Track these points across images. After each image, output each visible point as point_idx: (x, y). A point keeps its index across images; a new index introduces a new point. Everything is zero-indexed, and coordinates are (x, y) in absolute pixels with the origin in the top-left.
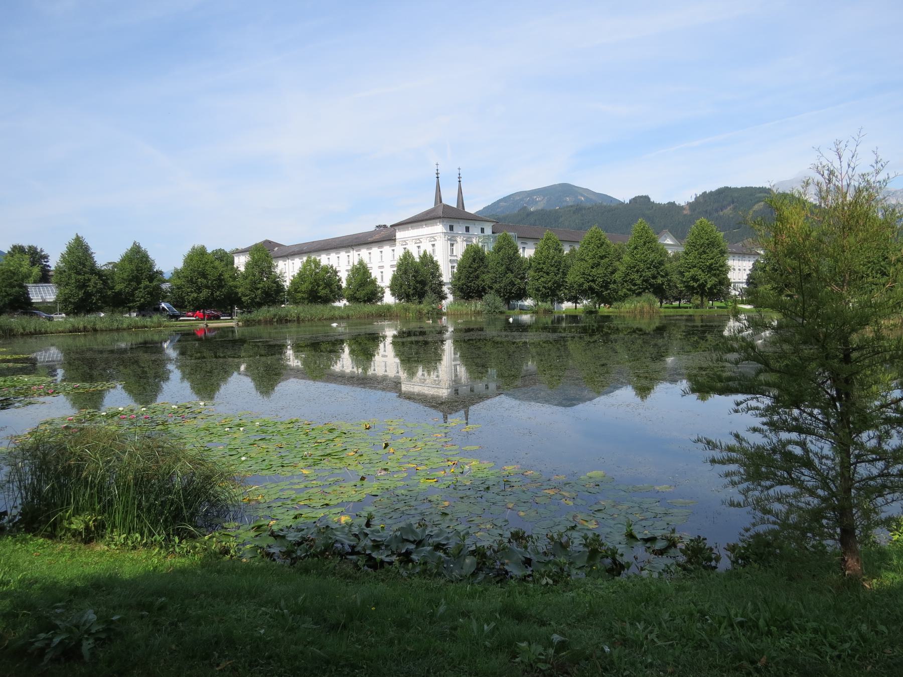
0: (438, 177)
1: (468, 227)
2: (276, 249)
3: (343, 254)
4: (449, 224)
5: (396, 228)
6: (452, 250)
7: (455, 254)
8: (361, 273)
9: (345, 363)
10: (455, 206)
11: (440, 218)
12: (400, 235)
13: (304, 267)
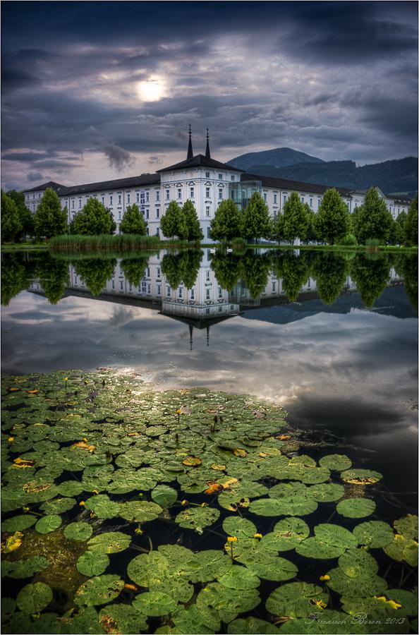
5: (161, 174)
6: (208, 195)
10: (194, 156)
12: (165, 179)
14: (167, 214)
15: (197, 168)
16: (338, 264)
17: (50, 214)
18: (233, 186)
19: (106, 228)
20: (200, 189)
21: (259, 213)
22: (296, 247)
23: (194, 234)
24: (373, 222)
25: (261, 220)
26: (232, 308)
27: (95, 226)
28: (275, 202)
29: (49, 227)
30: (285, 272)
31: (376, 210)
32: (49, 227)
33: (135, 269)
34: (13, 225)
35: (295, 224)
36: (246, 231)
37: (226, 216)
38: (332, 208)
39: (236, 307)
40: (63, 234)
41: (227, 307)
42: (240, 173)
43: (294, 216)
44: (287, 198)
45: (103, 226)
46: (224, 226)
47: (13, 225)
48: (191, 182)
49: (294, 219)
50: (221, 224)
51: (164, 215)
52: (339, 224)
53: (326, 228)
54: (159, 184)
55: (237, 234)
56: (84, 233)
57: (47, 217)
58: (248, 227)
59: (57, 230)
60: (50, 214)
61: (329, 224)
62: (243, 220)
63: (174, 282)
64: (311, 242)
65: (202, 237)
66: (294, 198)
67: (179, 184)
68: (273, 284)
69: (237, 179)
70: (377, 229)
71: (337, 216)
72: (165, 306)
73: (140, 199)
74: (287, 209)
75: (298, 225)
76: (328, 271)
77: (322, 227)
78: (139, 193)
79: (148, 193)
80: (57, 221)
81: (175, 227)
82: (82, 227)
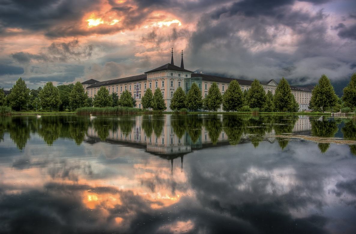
0: (182, 56)
1: (180, 74)
2: (96, 83)
3: (119, 86)
4: (185, 74)
5: (147, 74)
6: (172, 85)
7: (173, 86)
8: (127, 95)
9: (223, 89)
10: (180, 67)
11: (166, 69)
12: (149, 77)
13: (99, 93)
14: (145, 95)
15: (165, 71)
16: (238, 122)
17: (77, 95)
18: (187, 80)
19: (110, 103)
20: (167, 82)
21: (196, 94)
22: (221, 113)
23: (160, 107)
24: (256, 98)
25: (196, 99)
26: (186, 149)
27: (103, 102)
28: (205, 88)
29: (76, 102)
30: (209, 127)
31: (257, 92)
32: (76, 102)
33: (128, 126)
34: (56, 101)
35: (214, 100)
36: (188, 104)
37: (177, 96)
38: (234, 91)
39: (189, 148)
40: (85, 106)
41: (183, 148)
42: (191, 73)
43: (214, 95)
44: (248, 89)
45: (107, 102)
46: (176, 102)
47: (56, 101)
48: (163, 79)
49: (214, 97)
50: (175, 101)
51: (144, 96)
52: (238, 100)
53: (231, 102)
54: (146, 79)
55: (184, 106)
56: (97, 106)
57: (75, 97)
58: (190, 102)
59: (82, 104)
60: (77, 95)
61: (232, 100)
62: (187, 99)
63: (148, 133)
64: (230, 111)
65: (166, 108)
66: (214, 86)
67: (156, 80)
68: (205, 136)
69: (189, 76)
70: (258, 102)
71: (237, 95)
72: (149, 147)
73: (136, 88)
74: (210, 92)
75: (216, 101)
76: (233, 126)
77: (228, 101)
78: (136, 85)
79: (140, 85)
80: (81, 100)
81: (149, 102)
82: (96, 103)
